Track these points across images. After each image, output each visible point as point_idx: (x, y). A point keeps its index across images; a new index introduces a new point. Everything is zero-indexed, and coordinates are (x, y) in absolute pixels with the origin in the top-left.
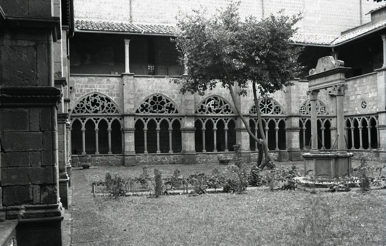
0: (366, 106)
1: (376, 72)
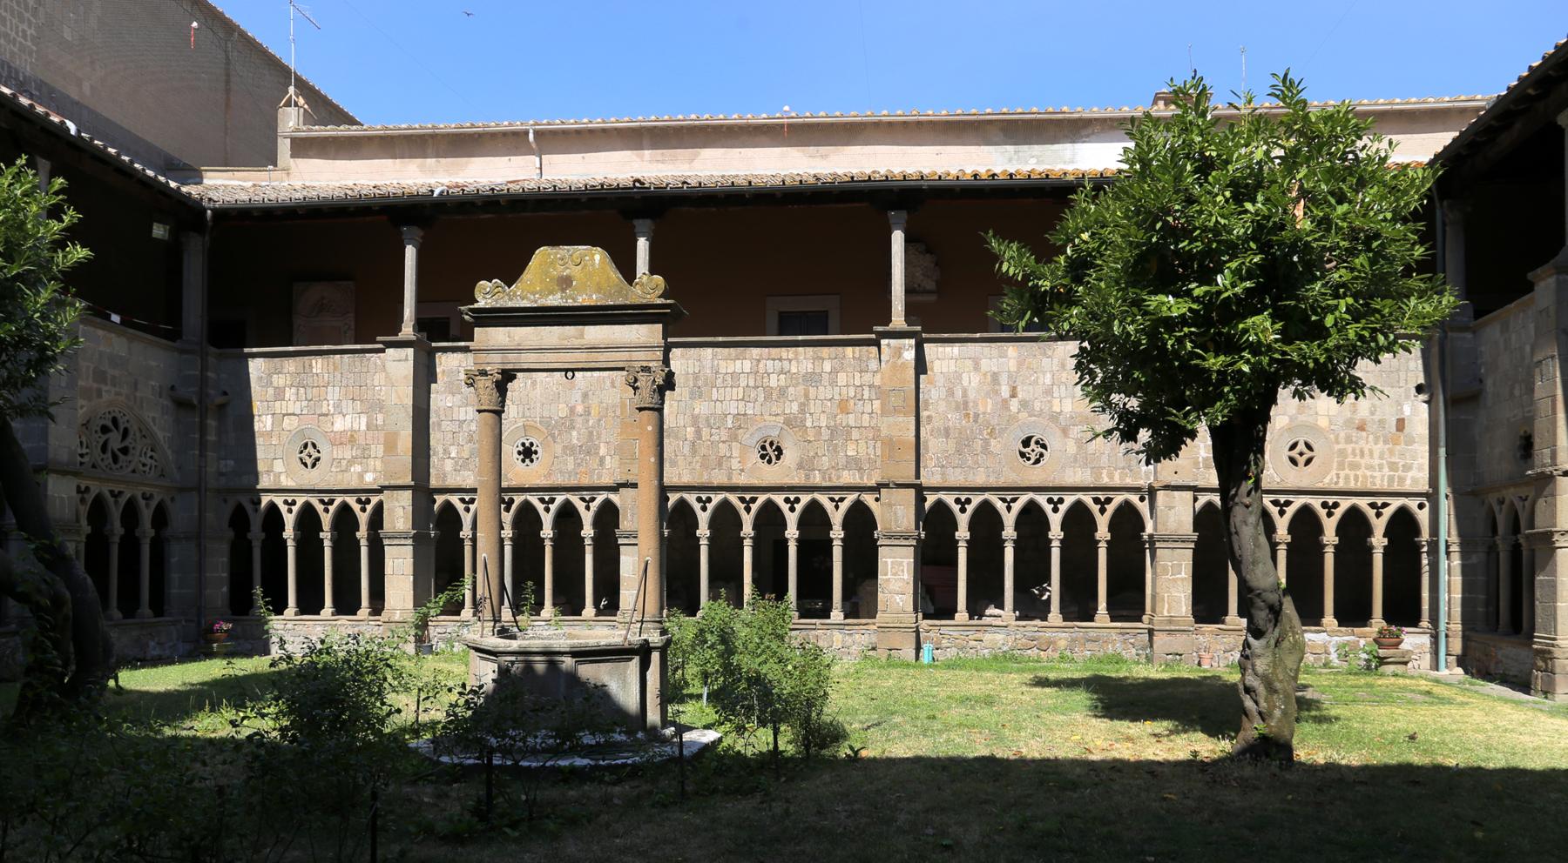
0: (318, 459)
1: (381, 346)
